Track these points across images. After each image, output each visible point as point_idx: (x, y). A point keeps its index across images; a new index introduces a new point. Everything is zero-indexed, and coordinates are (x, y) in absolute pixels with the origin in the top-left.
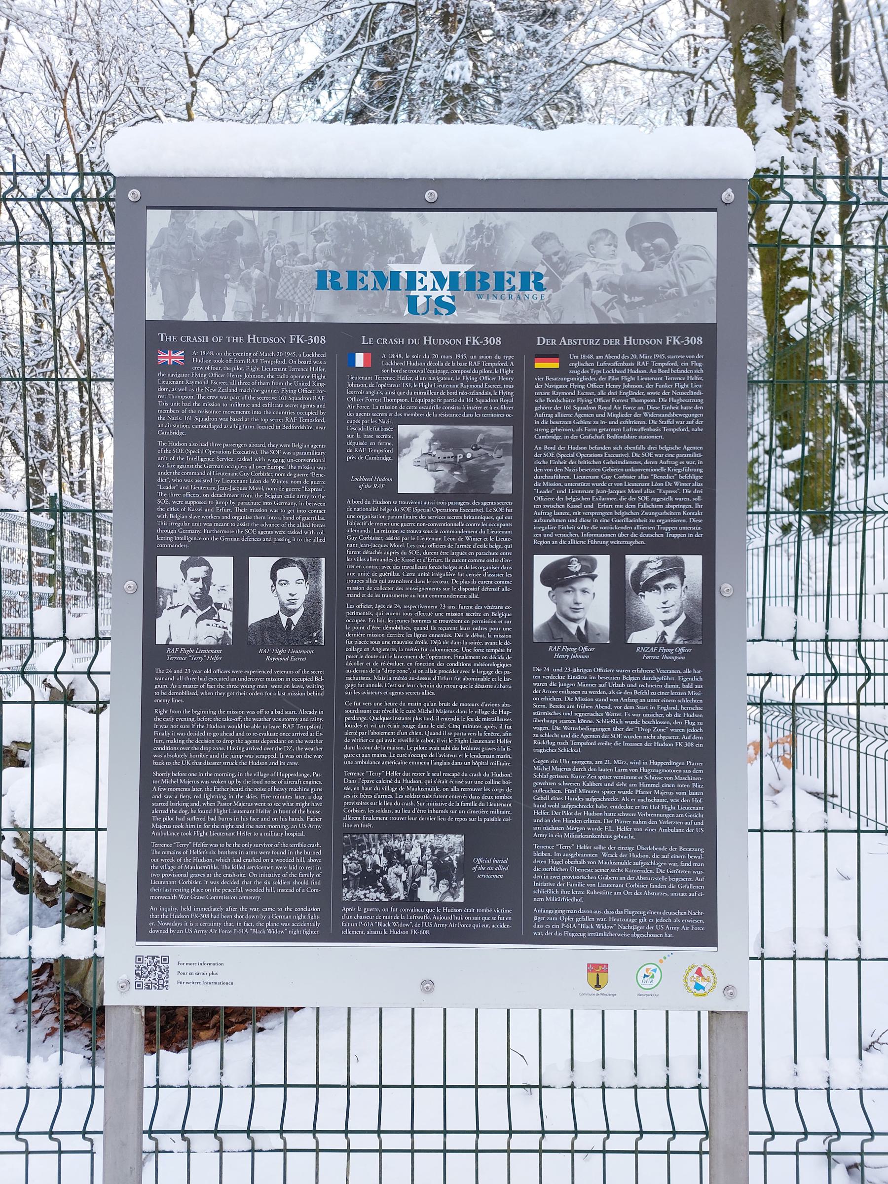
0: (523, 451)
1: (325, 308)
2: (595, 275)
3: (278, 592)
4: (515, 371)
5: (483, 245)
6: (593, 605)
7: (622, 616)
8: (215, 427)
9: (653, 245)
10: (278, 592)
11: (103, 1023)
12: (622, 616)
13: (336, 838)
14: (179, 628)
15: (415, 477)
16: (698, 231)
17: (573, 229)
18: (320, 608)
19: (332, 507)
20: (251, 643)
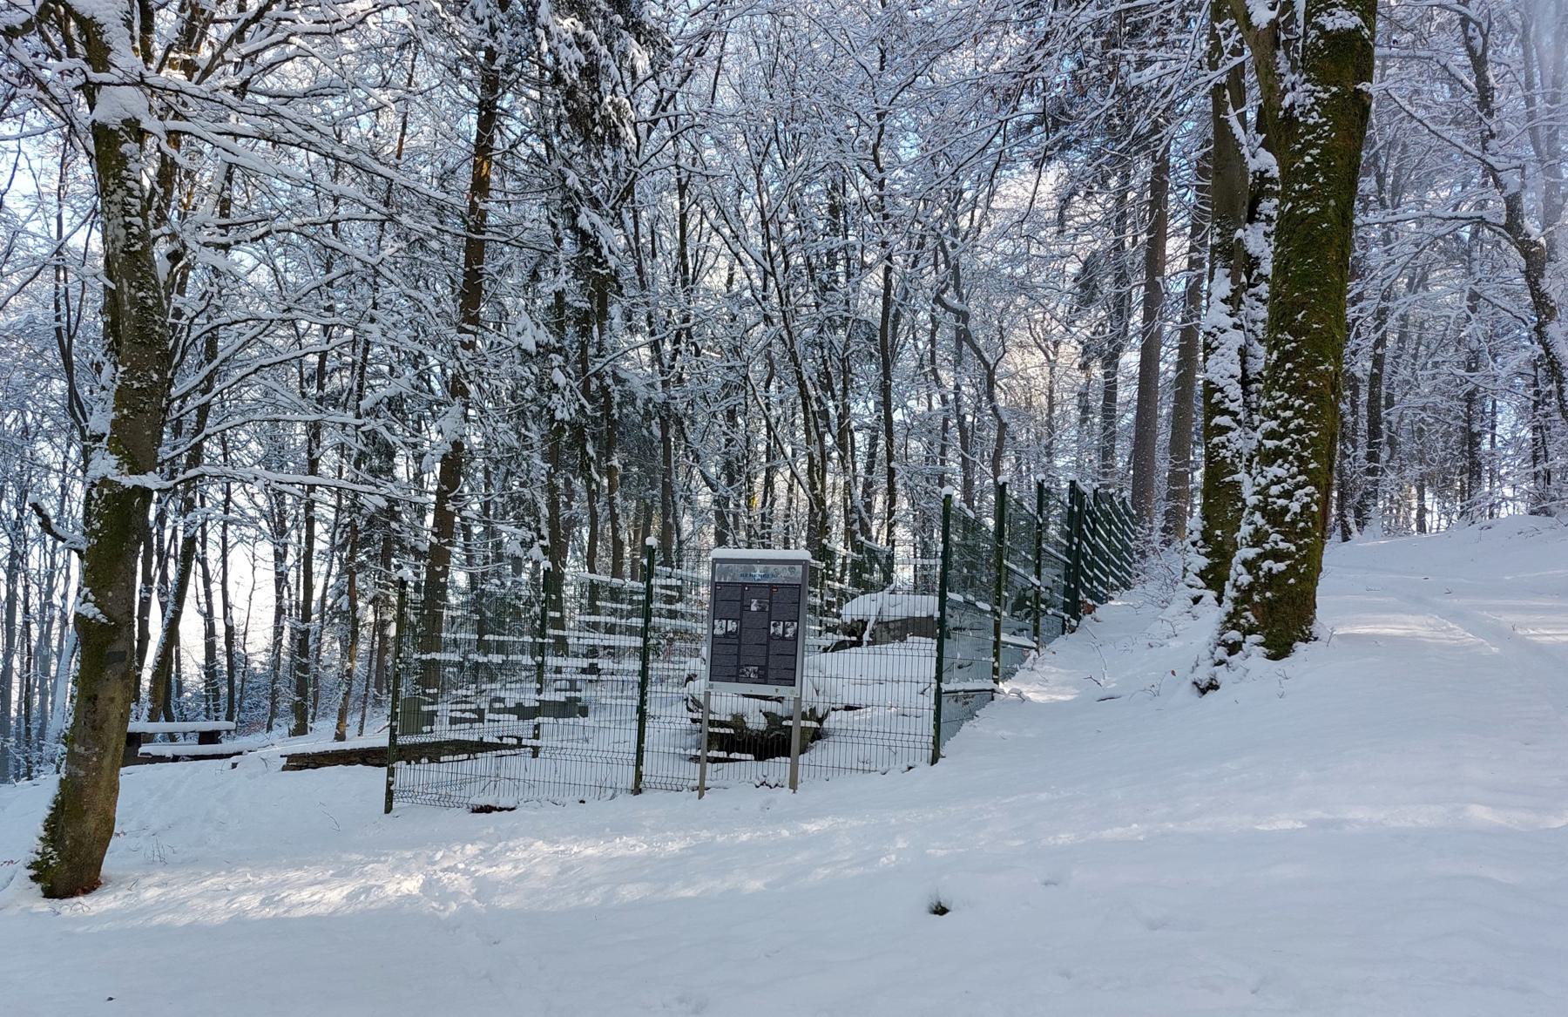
0: (770, 604)
1: (741, 580)
2: (783, 575)
3: (732, 626)
4: (771, 590)
5: (766, 570)
6: (780, 630)
7: (784, 632)
8: (152, 516)
9: (792, 570)
10: (732, 626)
11: (300, 768)
12: (784, 632)
13: (739, 667)
14: (718, 632)
15: (754, 608)
16: (799, 568)
17: (780, 567)
18: (133, 602)
19: (741, 613)
20: (727, 634)
